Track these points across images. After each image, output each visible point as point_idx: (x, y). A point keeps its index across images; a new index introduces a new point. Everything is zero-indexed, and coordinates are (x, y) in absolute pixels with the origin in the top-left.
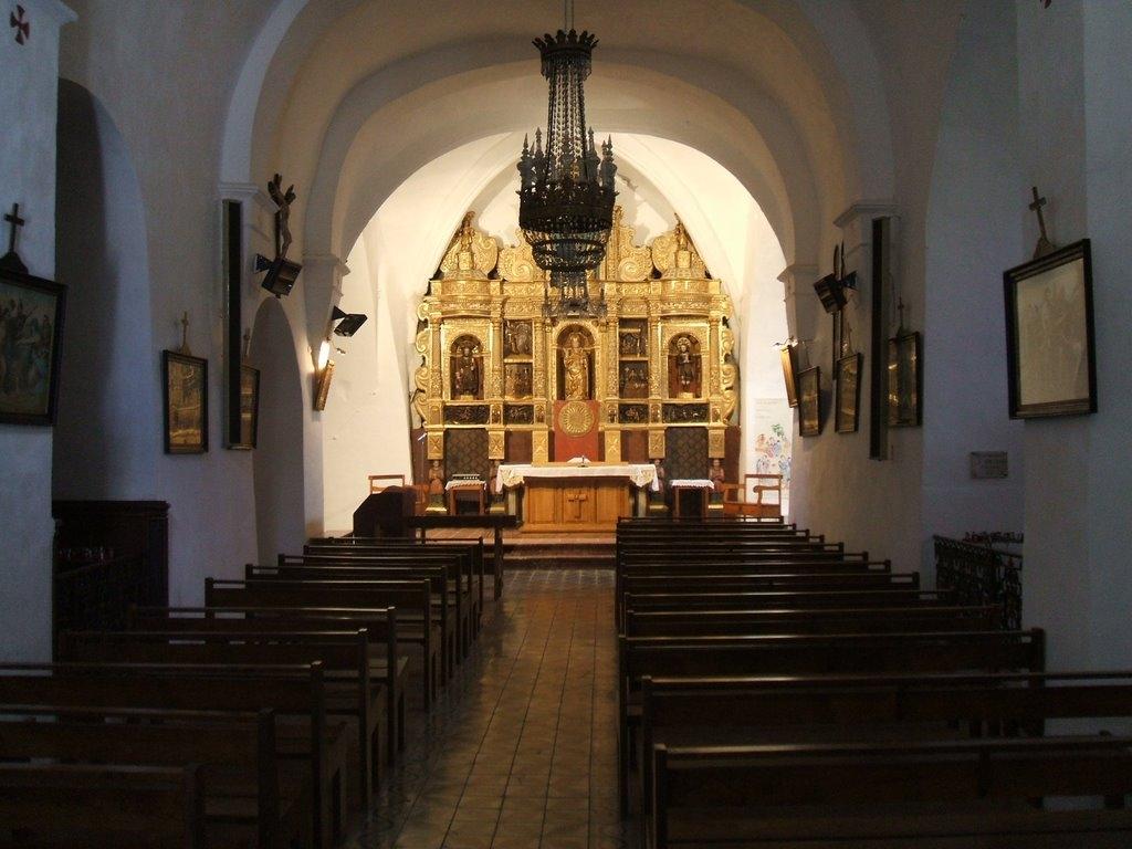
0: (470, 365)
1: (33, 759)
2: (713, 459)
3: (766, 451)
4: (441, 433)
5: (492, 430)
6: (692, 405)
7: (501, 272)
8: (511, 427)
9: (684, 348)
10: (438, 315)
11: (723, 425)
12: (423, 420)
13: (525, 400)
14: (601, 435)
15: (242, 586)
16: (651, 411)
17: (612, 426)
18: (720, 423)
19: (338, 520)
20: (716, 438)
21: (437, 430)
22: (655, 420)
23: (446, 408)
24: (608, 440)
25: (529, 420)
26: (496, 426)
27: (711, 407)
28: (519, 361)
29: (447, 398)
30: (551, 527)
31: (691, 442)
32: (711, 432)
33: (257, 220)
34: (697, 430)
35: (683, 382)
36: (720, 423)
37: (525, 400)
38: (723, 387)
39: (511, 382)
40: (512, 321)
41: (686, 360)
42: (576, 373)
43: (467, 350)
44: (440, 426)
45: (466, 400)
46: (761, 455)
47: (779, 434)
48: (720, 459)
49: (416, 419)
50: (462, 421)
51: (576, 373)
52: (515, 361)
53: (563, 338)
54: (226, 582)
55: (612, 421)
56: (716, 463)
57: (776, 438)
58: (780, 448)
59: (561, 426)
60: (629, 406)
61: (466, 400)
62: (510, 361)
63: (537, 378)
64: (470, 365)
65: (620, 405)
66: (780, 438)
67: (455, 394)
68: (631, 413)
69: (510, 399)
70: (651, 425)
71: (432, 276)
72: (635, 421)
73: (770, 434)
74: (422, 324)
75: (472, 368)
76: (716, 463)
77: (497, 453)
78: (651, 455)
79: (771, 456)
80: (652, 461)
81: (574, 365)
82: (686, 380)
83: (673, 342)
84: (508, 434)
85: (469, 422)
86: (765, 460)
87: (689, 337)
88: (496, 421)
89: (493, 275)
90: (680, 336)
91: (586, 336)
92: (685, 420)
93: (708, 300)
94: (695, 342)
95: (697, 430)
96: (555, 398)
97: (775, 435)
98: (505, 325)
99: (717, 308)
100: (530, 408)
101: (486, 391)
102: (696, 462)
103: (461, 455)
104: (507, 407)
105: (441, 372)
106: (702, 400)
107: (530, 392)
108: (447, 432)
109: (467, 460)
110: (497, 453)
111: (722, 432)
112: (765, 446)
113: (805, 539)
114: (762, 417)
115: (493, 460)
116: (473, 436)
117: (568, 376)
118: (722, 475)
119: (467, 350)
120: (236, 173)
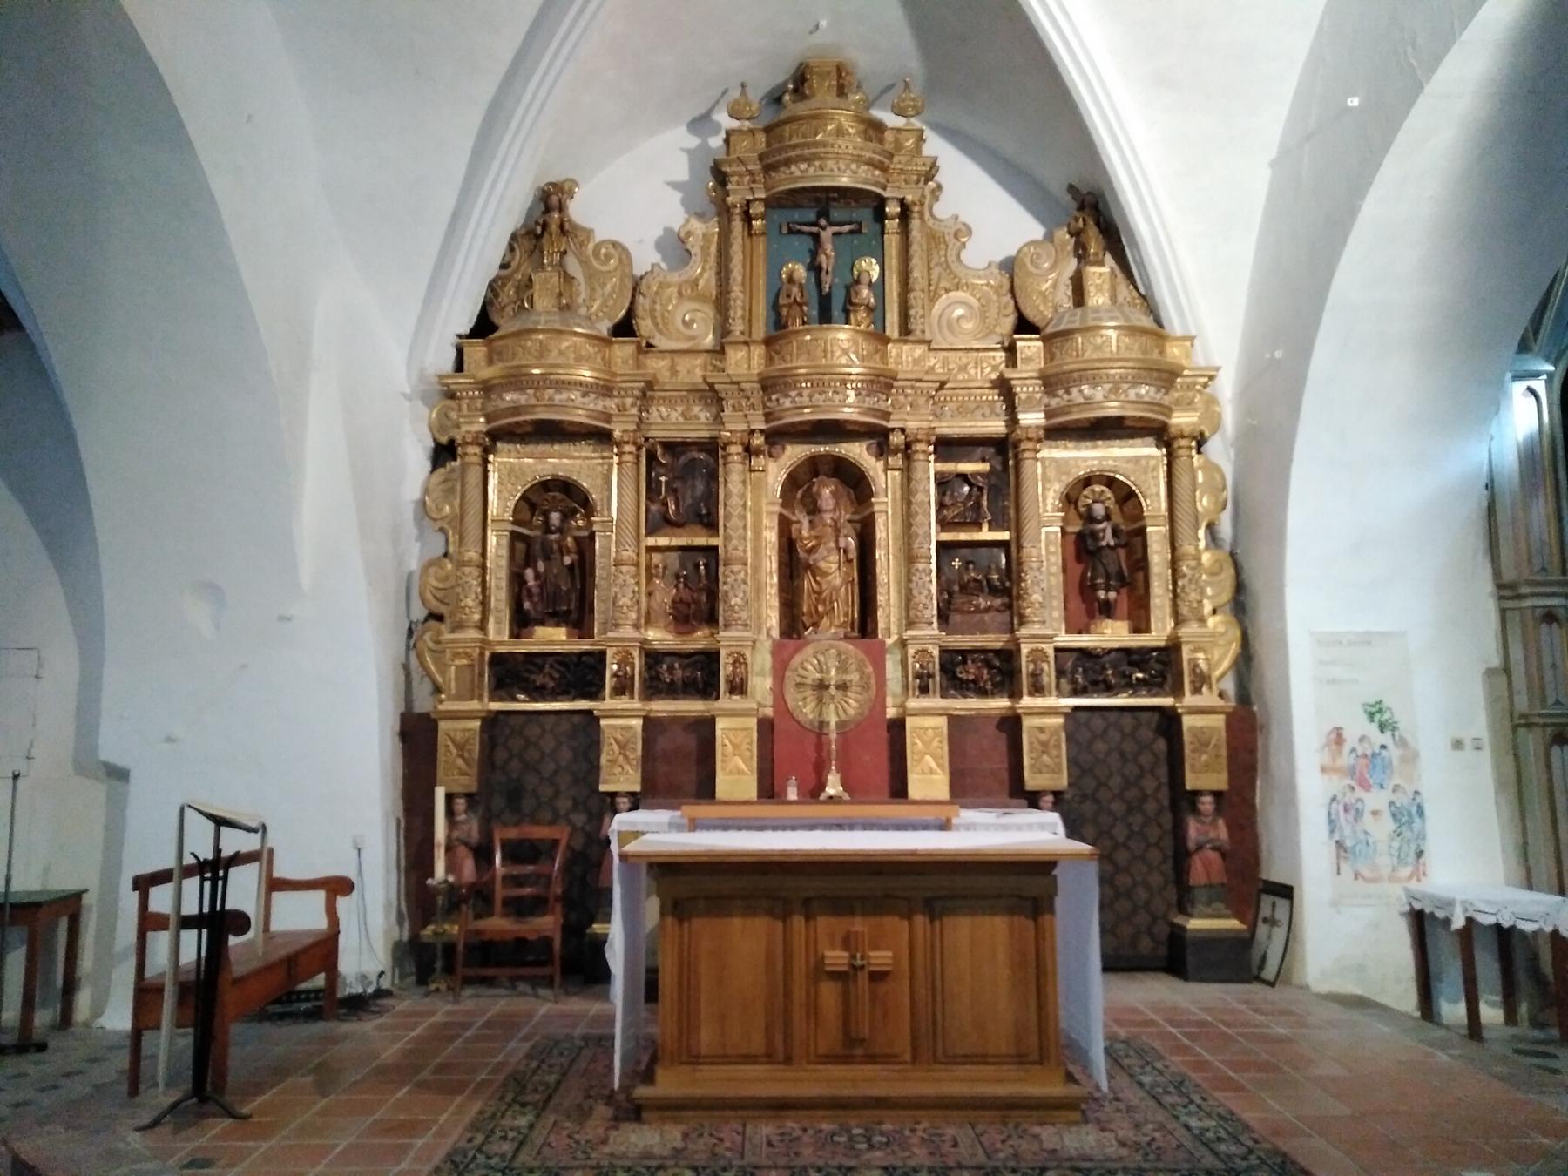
0: (563, 550)
2: (1196, 793)
3: (1351, 772)
4: (477, 724)
5: (612, 714)
6: (1126, 652)
7: (644, 325)
8: (663, 707)
9: (1099, 510)
10: (480, 424)
11: (1219, 702)
12: (437, 690)
13: (699, 640)
14: (897, 728)
15: (205, 932)
16: (1025, 666)
18: (1207, 698)
20: (1202, 743)
21: (468, 716)
22: (1038, 689)
23: (498, 660)
24: (914, 743)
25: (708, 689)
26: (623, 703)
27: (1186, 653)
29: (499, 633)
30: (761, 1081)
31: (1128, 747)
32: (1188, 721)
33: (1522, 1046)
34: (1144, 716)
36: (1207, 698)
39: (665, 594)
41: (1109, 540)
42: (834, 570)
44: (474, 705)
45: (553, 638)
46: (1338, 784)
47: (1382, 727)
48: (1217, 795)
49: (422, 691)
50: (538, 693)
51: (834, 570)
52: (676, 542)
53: (798, 486)
54: (1170, 244)
55: (924, 690)
56: (1207, 803)
57: (1378, 738)
58: (1387, 767)
60: (964, 653)
61: (553, 638)
62: (663, 541)
64: (563, 550)
66: (1386, 738)
67: (521, 623)
68: (969, 671)
69: (659, 636)
70: (1027, 701)
71: (465, 330)
72: (983, 693)
73: (1358, 727)
74: (443, 453)
75: (567, 560)
76: (1207, 803)
77: (621, 776)
78: (1032, 781)
79: (1365, 786)
80: (1033, 800)
81: (822, 551)
82: (1107, 590)
83: (1070, 499)
84: (652, 725)
85: (554, 695)
86: (1350, 798)
87: (1110, 482)
88: (622, 689)
89: (625, 328)
90: (1087, 481)
91: (856, 484)
92: (1109, 689)
93: (1167, 376)
94: (1127, 497)
97: (1373, 730)
98: (652, 457)
99: (1189, 405)
100: (710, 659)
101: (598, 616)
103: (531, 780)
104: (653, 657)
105: (483, 567)
108: (492, 722)
110: (621, 776)
111: (1218, 721)
112: (1346, 759)
114: (1333, 681)
115: (613, 795)
116: (565, 726)
120: (891, 712)
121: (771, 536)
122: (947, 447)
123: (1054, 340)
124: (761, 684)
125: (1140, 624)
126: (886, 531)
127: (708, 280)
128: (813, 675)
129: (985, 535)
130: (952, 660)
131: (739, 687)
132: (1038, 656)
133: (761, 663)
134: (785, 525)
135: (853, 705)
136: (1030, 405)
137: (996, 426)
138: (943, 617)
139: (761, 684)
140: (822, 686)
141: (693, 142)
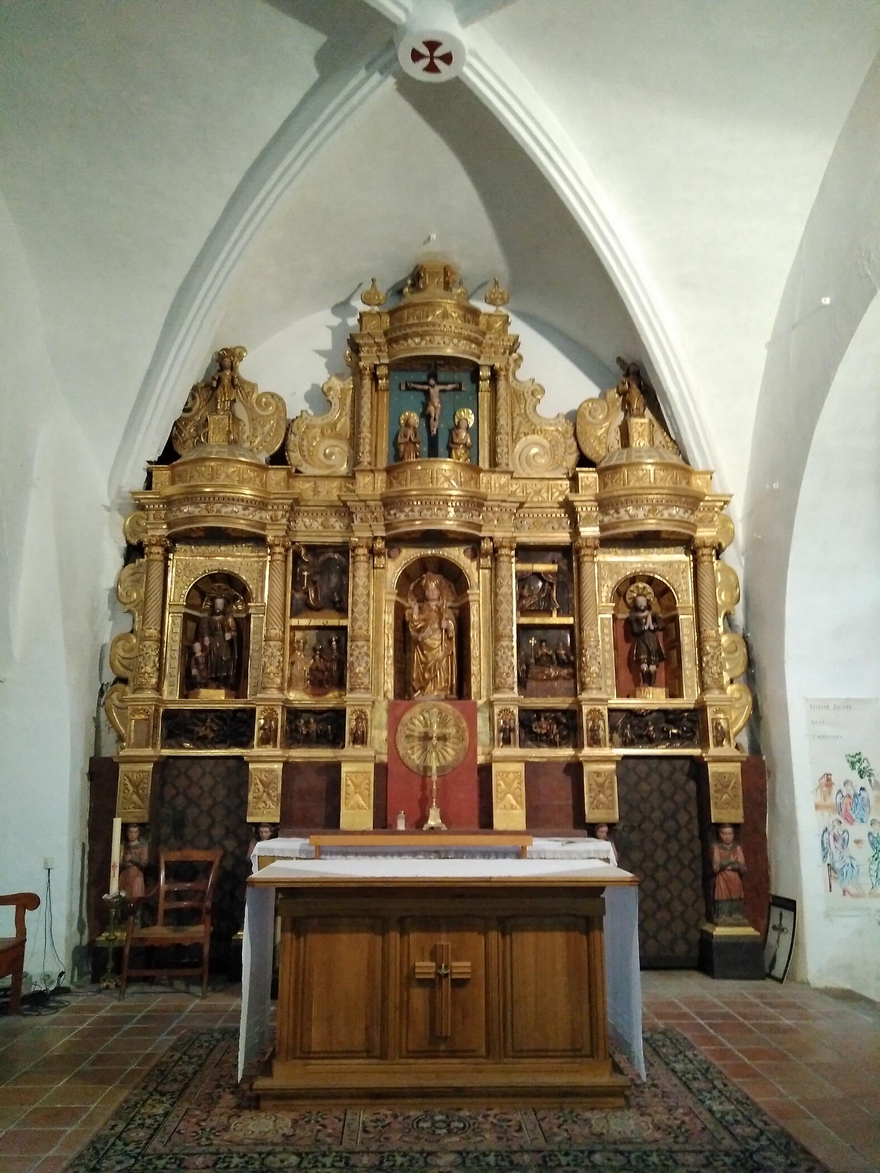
0: (225, 628)
1: (111, 623)
2: (719, 826)
3: (839, 809)
4: (150, 767)
5: (259, 760)
6: (664, 712)
7: (294, 456)
8: (299, 754)
13: (330, 700)
14: (485, 771)
17: (508, 751)
19: (627, 875)
20: (724, 782)
22: (595, 742)
23: (170, 716)
24: (498, 784)
25: (337, 741)
26: (268, 751)
28: (319, 622)
29: (171, 693)
32: (712, 768)
34: (678, 763)
35: (645, 667)
36: (727, 750)
37: (330, 700)
38: (726, 678)
39: (304, 664)
40: (312, 549)
41: (649, 624)
43: (220, 602)
44: (149, 751)
46: (829, 818)
47: (861, 774)
48: (735, 826)
50: (201, 742)
55: (507, 742)
56: (728, 833)
57: (858, 782)
59: (401, 752)
60: (539, 712)
62: (304, 622)
63: (356, 652)
64: (225, 628)
65: (522, 710)
66: (865, 782)
67: (189, 685)
68: (542, 727)
69: (298, 697)
70: (587, 751)
72: (553, 744)
73: (842, 773)
75: (228, 636)
76: (728, 833)
78: (591, 815)
79: (851, 821)
80: (592, 831)
85: (214, 744)
86: (838, 830)
87: (651, 581)
88: (268, 739)
90: (633, 579)
92: (651, 742)
94: (663, 591)
95: (678, 763)
96: (391, 695)
99: (710, 523)
100: (338, 715)
102: (678, 831)
104: (293, 714)
105: (161, 641)
106: (688, 700)
107: (340, 684)
109: (205, 822)
112: (834, 799)
113: (171, 979)
115: (258, 825)
116: (221, 769)
117: (417, 655)
118: (741, 859)
119: (220, 602)
121: (389, 618)
122: (525, 552)
123: (606, 472)
124: (379, 735)
125: (675, 692)
126: (478, 616)
127: (344, 425)
128: (419, 728)
129: (555, 620)
130: (528, 717)
131: (360, 739)
132: (595, 715)
133: (380, 717)
134: (400, 611)
135: (450, 753)
136: (588, 521)
137: (563, 537)
138: (522, 683)
139: (379, 735)
140: (426, 738)
141: (336, 321)
